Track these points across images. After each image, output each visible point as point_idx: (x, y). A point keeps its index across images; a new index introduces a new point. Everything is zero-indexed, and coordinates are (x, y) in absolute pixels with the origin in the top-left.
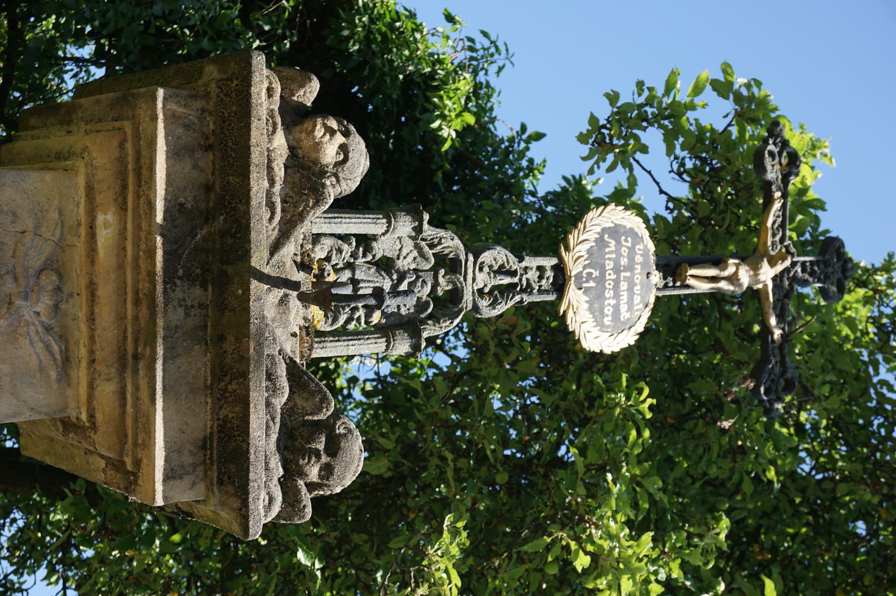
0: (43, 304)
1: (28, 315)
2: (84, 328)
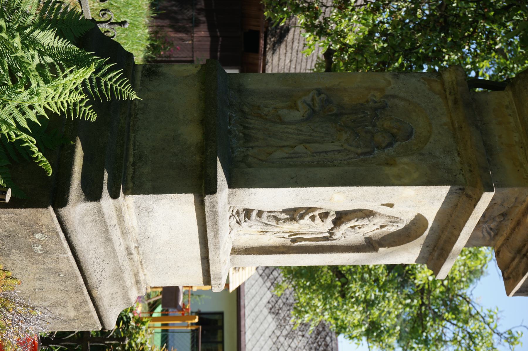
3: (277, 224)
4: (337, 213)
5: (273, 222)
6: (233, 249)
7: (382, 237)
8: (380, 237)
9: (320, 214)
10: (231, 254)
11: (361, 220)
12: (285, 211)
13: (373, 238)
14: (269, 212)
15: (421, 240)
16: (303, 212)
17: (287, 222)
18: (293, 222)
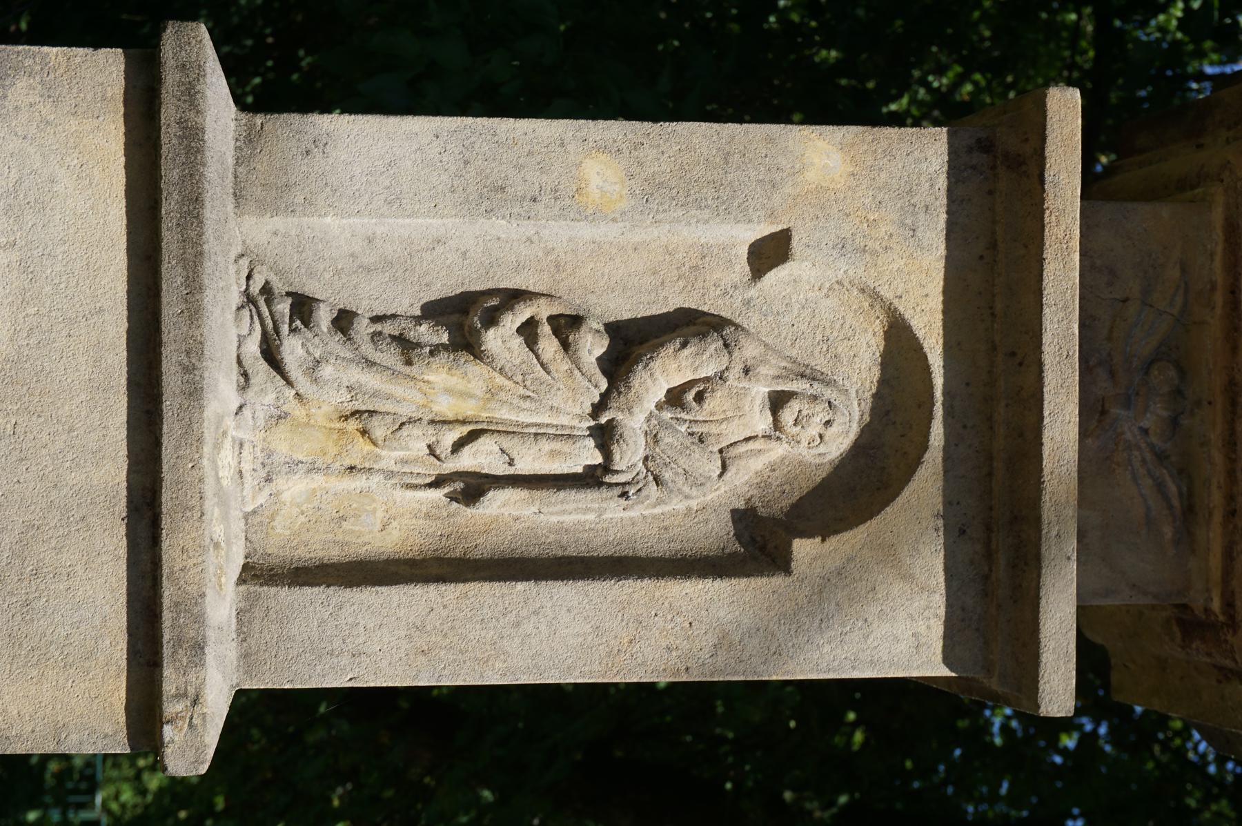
0: (1154, 416)
1: (1130, 433)
2: (1218, 457)
3: (409, 363)
4: (615, 330)
5: (390, 356)
6: (246, 567)
7: (794, 506)
8: (786, 503)
9: (552, 319)
10: (241, 581)
11: (695, 340)
12: (434, 311)
13: (762, 512)
14: (376, 319)
15: (927, 485)
16: (494, 302)
17: (443, 356)
18: (464, 356)
